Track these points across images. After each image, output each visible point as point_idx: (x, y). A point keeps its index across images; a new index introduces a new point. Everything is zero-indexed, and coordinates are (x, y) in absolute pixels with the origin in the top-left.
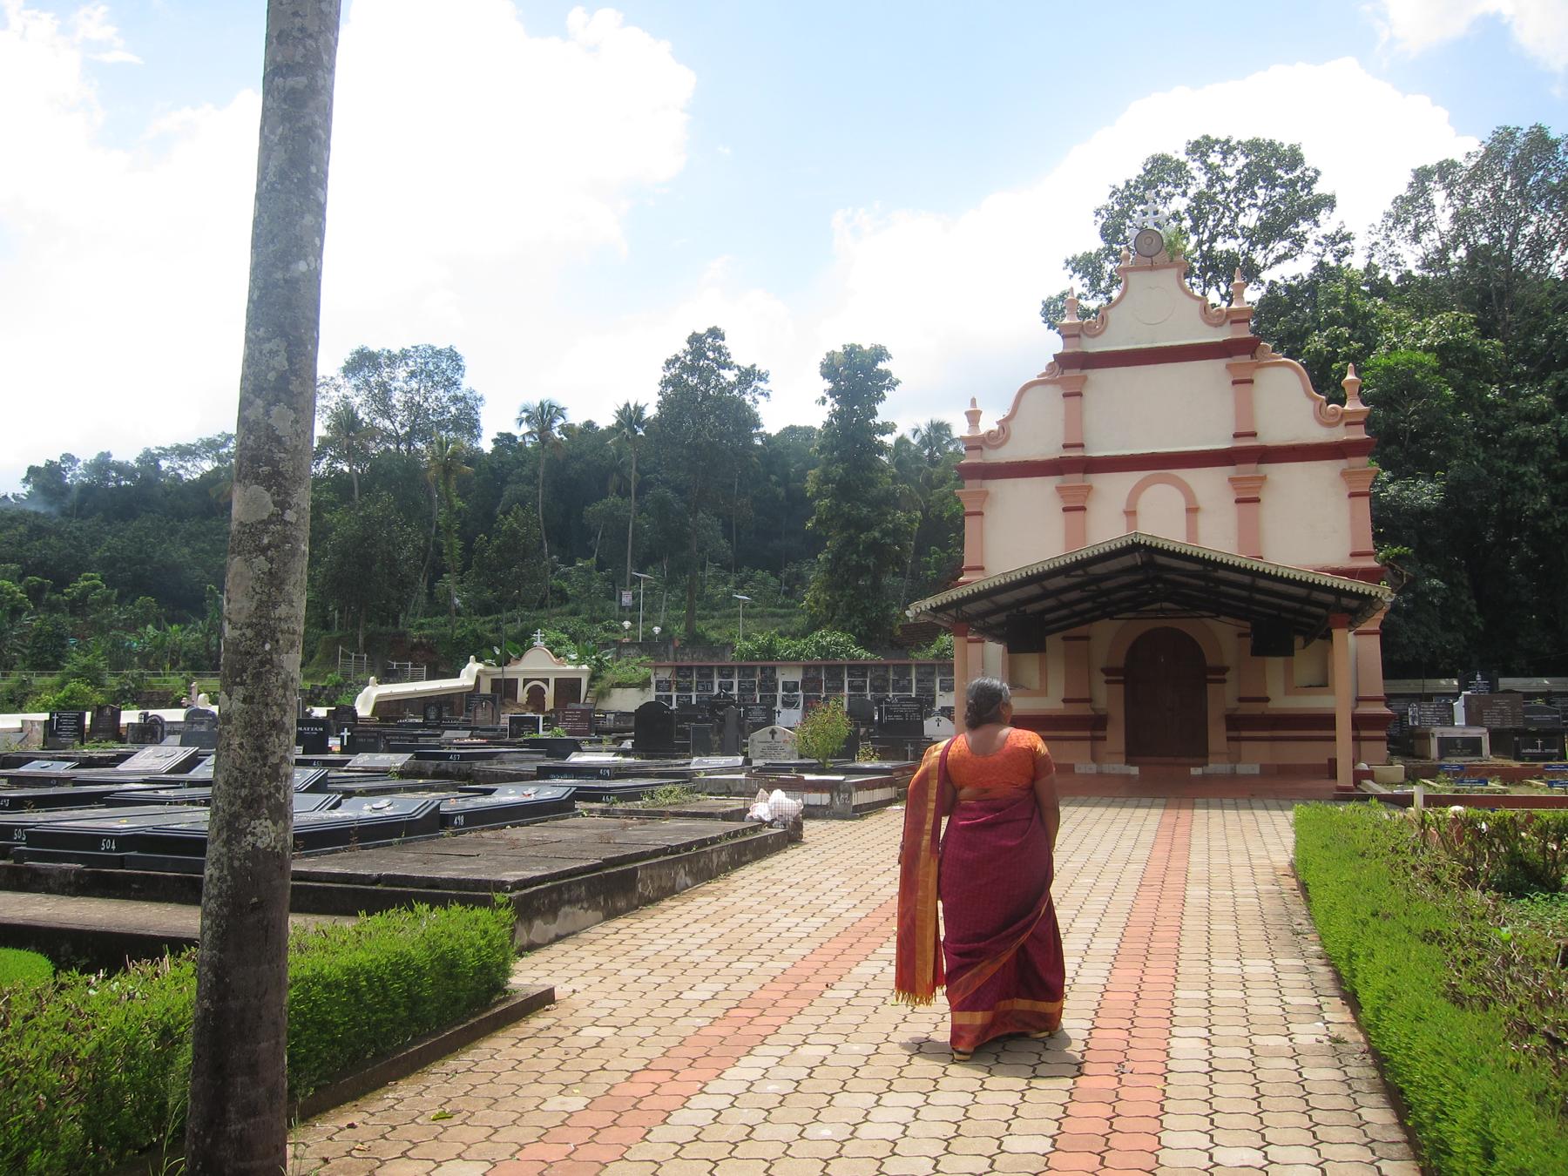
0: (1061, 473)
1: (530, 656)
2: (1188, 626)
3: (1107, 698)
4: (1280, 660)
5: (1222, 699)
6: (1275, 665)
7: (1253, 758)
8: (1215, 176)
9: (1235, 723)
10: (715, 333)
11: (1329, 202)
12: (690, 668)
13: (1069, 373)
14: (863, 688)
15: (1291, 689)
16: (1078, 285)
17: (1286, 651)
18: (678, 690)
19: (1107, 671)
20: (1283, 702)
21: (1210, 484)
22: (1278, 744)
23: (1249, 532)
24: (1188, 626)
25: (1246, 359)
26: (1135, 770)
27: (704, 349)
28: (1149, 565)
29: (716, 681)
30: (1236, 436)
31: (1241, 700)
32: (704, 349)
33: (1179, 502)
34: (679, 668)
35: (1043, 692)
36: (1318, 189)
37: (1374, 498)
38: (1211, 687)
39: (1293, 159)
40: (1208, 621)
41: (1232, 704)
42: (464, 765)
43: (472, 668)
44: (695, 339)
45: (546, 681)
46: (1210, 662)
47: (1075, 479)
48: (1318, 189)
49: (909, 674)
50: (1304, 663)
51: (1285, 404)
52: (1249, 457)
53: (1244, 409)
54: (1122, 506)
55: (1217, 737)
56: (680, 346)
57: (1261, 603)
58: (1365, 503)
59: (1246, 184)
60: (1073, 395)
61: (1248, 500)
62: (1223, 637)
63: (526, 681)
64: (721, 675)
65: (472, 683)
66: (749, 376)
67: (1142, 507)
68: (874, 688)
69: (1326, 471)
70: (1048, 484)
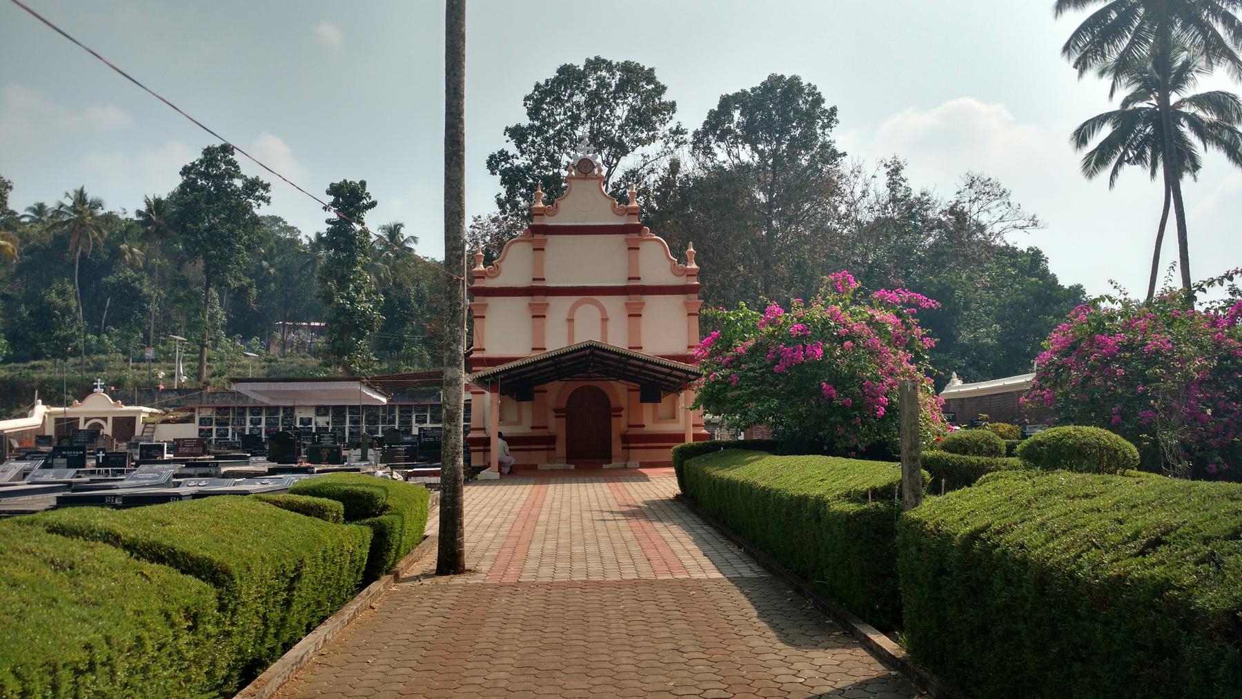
0: (531, 295)
1: (90, 399)
2: (598, 384)
3: (556, 426)
4: (650, 405)
5: (619, 426)
6: (648, 408)
7: (638, 455)
8: (602, 84)
9: (626, 439)
10: (227, 149)
11: (672, 107)
12: (226, 408)
13: (537, 237)
14: (260, 422)
15: (657, 419)
16: (512, 148)
17: (656, 399)
18: (217, 424)
19: (556, 410)
20: (652, 427)
21: (615, 305)
22: (649, 451)
23: (634, 333)
24: (598, 384)
25: (636, 236)
26: (572, 467)
27: (217, 160)
28: (592, 354)
29: (248, 418)
30: (630, 279)
31: (630, 426)
32: (217, 160)
33: (597, 315)
34: (218, 408)
35: (519, 422)
36: (666, 98)
37: (699, 315)
38: (613, 419)
39: (649, 76)
40: (613, 383)
41: (623, 427)
42: (191, 471)
43: (40, 410)
44: (208, 151)
45: (105, 419)
46: (613, 405)
47: (539, 299)
48: (666, 98)
49: (394, 411)
50: (664, 406)
51: (655, 261)
52: (634, 291)
53: (633, 264)
54: (565, 316)
55: (617, 447)
56: (196, 156)
57: (644, 374)
58: (695, 320)
59: (621, 87)
60: (539, 249)
61: (635, 315)
62: (620, 391)
63: (87, 420)
64: (252, 413)
65: (40, 421)
66: (253, 186)
67: (576, 317)
68: (368, 422)
69: (678, 300)
70: (523, 301)
